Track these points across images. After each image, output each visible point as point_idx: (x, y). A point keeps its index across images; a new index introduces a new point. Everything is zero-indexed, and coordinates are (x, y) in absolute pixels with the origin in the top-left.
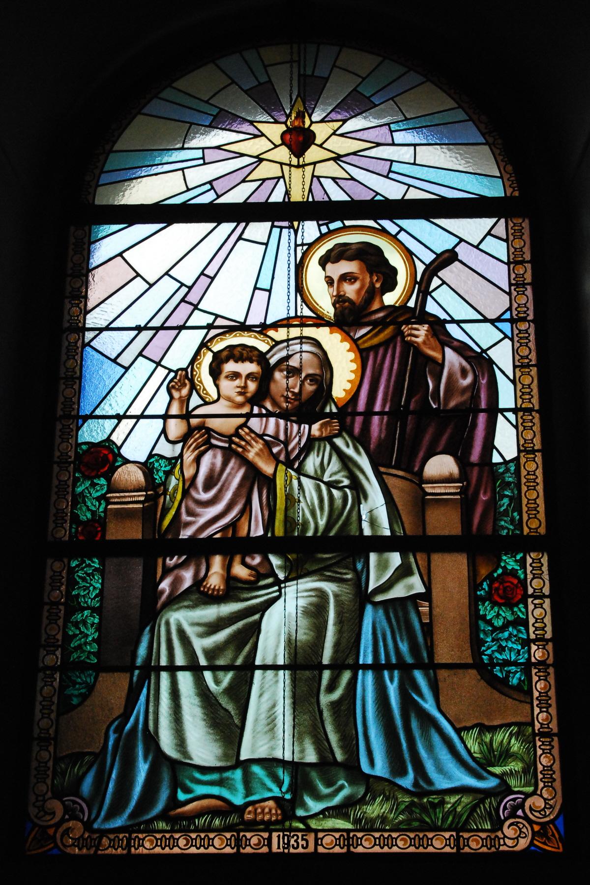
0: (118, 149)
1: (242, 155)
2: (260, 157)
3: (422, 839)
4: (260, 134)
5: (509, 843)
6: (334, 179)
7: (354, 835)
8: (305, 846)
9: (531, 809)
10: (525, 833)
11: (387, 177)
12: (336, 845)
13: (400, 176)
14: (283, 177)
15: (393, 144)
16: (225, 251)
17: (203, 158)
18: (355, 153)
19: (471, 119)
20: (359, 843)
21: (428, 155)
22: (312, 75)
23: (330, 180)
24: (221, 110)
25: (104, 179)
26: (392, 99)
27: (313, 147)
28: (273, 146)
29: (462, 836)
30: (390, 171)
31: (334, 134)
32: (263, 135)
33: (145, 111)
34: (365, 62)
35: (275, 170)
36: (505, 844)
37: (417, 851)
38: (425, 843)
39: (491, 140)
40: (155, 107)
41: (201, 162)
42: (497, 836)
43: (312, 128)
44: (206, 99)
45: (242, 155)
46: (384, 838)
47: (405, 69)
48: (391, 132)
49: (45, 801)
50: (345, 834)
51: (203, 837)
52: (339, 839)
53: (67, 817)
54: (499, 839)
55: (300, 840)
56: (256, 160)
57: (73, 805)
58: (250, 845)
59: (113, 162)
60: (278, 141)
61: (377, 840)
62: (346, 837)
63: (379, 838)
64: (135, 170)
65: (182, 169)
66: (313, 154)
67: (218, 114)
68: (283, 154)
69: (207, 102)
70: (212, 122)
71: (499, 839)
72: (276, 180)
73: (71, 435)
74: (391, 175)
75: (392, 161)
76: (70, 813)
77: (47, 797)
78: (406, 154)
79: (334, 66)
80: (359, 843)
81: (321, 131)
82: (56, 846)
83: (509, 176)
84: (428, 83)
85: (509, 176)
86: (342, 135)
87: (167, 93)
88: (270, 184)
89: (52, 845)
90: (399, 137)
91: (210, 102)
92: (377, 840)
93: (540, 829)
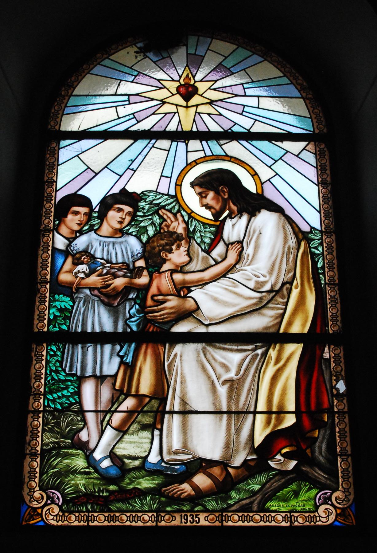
0: (76, 94)
1: (152, 99)
2: (164, 100)
3: (135, 517)
4: (163, 87)
5: (324, 520)
6: (209, 114)
7: (92, 515)
8: (198, 521)
9: (336, 499)
10: (331, 512)
11: (241, 114)
12: (216, 520)
13: (249, 114)
14: (178, 112)
15: (245, 96)
16: (143, 156)
17: (129, 101)
18: (221, 100)
19: (292, 83)
20: (95, 519)
21: (266, 103)
22: (195, 54)
23: (207, 115)
24: (139, 72)
25: (67, 110)
26: (244, 70)
27: (196, 96)
28: (171, 95)
29: (293, 515)
30: (243, 111)
31: (209, 88)
32: (165, 87)
33: (92, 72)
34: (225, 47)
35: (173, 109)
36: (320, 520)
37: (109, 524)
38: (136, 518)
39: (304, 95)
40: (98, 69)
41: (127, 103)
42: (315, 515)
43: (195, 85)
44: (130, 66)
45: (152, 99)
46: (245, 516)
47: (251, 53)
48: (244, 89)
49: (34, 492)
50: (288, 514)
51: (134, 515)
52: (285, 517)
53: (49, 502)
54: (316, 517)
55: (194, 518)
56: (161, 102)
57: (53, 495)
58: (164, 520)
59: (72, 101)
60: (175, 92)
61: (240, 518)
62: (155, 516)
63: (242, 517)
64: (80, 107)
65: (116, 107)
66: (196, 100)
67: (137, 75)
68: (178, 99)
69: (131, 68)
70: (134, 79)
71: (316, 517)
72: (174, 114)
73: (328, 265)
74: (244, 113)
75: (244, 106)
76: (327, 501)
77: (35, 490)
78: (253, 102)
79: (208, 49)
80: (95, 519)
81: (202, 87)
82: (43, 520)
83: (315, 116)
84: (266, 62)
85: (315, 116)
86: (215, 89)
87: (106, 62)
88: (169, 116)
89: (40, 519)
90: (249, 92)
91: (132, 68)
92: (240, 518)
93: (342, 512)
